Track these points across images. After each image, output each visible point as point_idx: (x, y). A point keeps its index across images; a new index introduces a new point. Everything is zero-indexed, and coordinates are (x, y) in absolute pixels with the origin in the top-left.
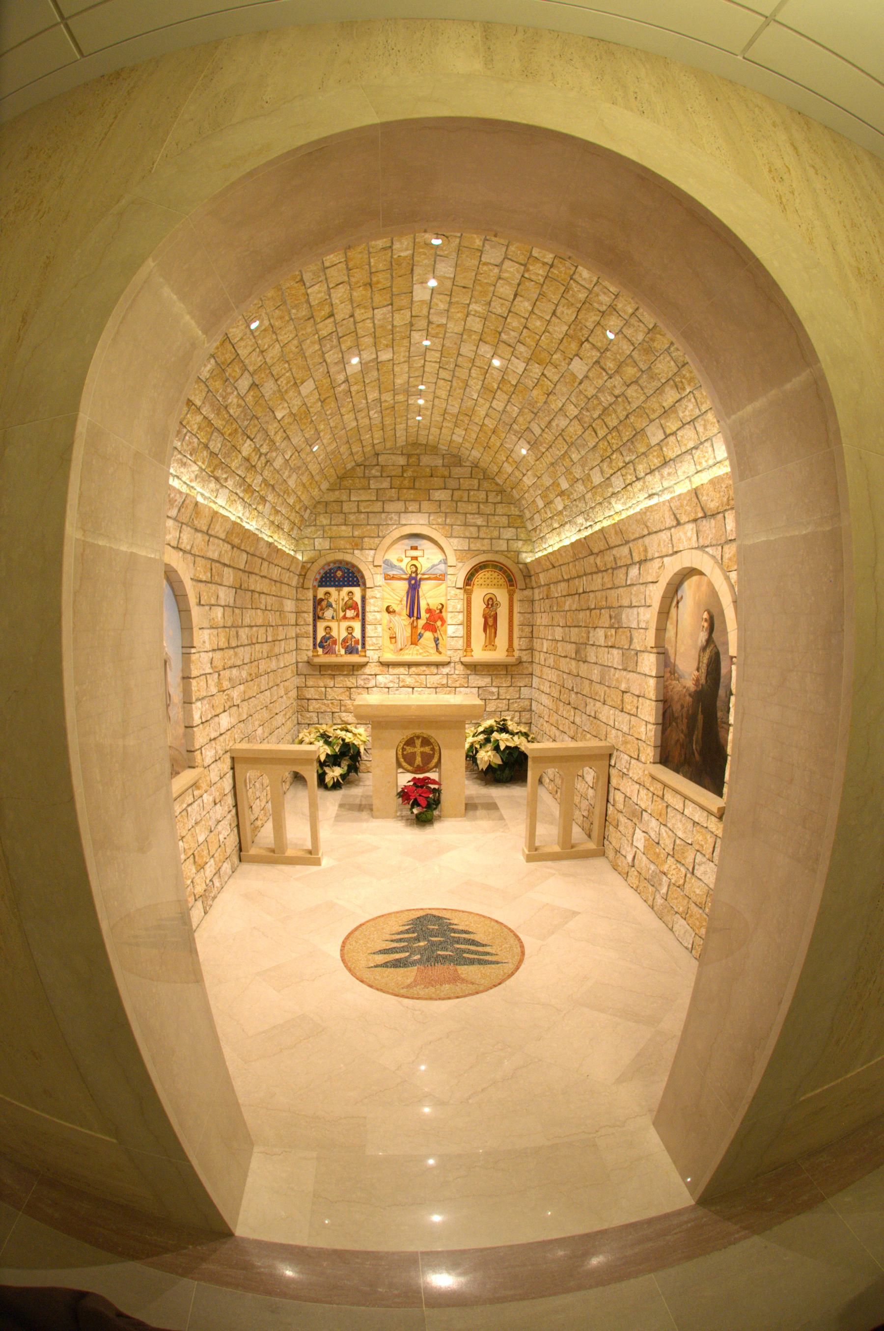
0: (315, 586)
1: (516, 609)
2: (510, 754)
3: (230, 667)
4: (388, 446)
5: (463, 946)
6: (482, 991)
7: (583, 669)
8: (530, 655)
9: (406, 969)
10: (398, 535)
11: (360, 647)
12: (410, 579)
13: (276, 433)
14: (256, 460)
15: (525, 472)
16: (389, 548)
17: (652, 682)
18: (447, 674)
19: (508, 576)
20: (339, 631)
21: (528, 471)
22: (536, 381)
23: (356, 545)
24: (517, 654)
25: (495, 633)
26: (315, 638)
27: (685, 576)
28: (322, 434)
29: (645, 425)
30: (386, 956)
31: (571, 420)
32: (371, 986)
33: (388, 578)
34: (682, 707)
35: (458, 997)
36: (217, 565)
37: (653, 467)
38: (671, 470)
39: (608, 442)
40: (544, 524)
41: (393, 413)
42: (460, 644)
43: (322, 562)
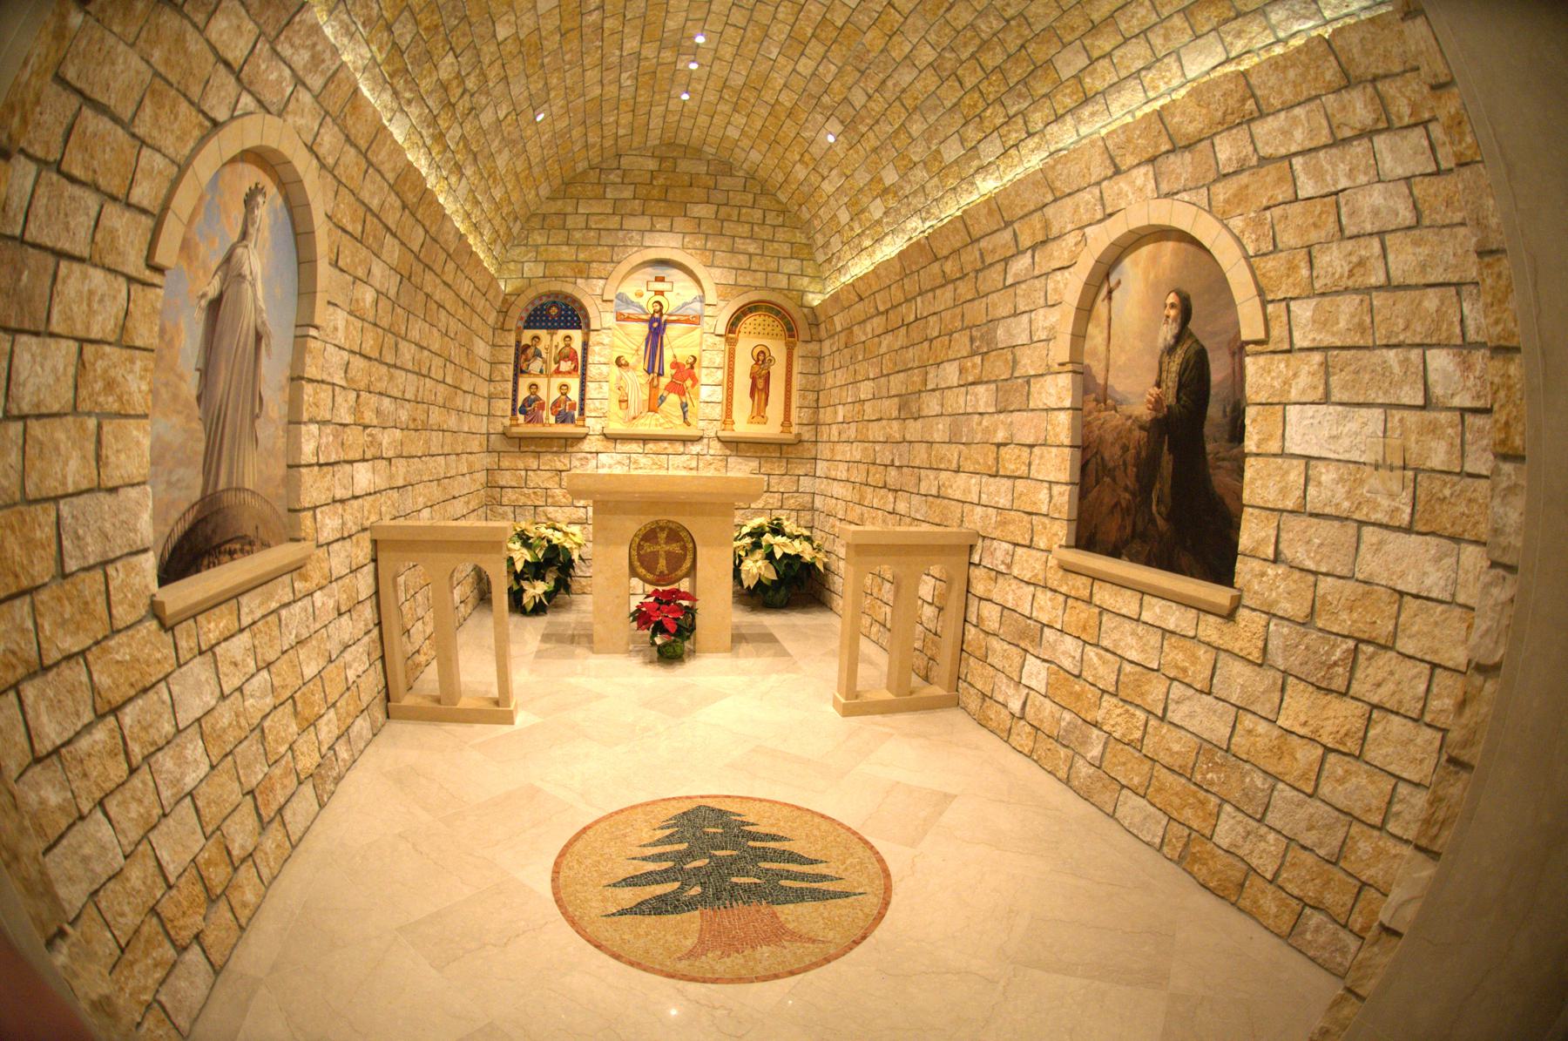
0: (519, 328)
1: (796, 369)
2: (789, 566)
3: (380, 394)
4: (635, 145)
5: (775, 866)
6: (836, 957)
7: (914, 429)
8: (813, 432)
9: (679, 917)
10: (639, 261)
11: (576, 414)
12: (651, 321)
13: (492, 63)
14: (458, 95)
15: (826, 174)
16: (624, 278)
17: (1064, 419)
18: (698, 454)
19: (788, 324)
20: (549, 391)
21: (832, 169)
22: (876, 15)
23: (580, 272)
24: (795, 429)
25: (767, 400)
26: (515, 400)
27: (1125, 249)
28: (552, 94)
29: (1053, 52)
30: (637, 889)
31: (921, 72)
32: (617, 957)
33: (621, 318)
34: (1125, 449)
35: (792, 973)
36: (375, 220)
37: (1060, 112)
38: (1097, 107)
39: (981, 92)
40: (846, 247)
41: (651, 82)
42: (717, 412)
43: (531, 294)
